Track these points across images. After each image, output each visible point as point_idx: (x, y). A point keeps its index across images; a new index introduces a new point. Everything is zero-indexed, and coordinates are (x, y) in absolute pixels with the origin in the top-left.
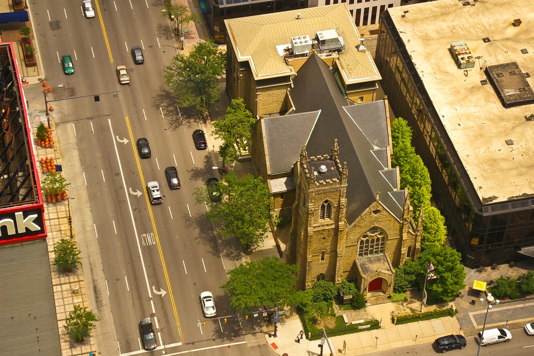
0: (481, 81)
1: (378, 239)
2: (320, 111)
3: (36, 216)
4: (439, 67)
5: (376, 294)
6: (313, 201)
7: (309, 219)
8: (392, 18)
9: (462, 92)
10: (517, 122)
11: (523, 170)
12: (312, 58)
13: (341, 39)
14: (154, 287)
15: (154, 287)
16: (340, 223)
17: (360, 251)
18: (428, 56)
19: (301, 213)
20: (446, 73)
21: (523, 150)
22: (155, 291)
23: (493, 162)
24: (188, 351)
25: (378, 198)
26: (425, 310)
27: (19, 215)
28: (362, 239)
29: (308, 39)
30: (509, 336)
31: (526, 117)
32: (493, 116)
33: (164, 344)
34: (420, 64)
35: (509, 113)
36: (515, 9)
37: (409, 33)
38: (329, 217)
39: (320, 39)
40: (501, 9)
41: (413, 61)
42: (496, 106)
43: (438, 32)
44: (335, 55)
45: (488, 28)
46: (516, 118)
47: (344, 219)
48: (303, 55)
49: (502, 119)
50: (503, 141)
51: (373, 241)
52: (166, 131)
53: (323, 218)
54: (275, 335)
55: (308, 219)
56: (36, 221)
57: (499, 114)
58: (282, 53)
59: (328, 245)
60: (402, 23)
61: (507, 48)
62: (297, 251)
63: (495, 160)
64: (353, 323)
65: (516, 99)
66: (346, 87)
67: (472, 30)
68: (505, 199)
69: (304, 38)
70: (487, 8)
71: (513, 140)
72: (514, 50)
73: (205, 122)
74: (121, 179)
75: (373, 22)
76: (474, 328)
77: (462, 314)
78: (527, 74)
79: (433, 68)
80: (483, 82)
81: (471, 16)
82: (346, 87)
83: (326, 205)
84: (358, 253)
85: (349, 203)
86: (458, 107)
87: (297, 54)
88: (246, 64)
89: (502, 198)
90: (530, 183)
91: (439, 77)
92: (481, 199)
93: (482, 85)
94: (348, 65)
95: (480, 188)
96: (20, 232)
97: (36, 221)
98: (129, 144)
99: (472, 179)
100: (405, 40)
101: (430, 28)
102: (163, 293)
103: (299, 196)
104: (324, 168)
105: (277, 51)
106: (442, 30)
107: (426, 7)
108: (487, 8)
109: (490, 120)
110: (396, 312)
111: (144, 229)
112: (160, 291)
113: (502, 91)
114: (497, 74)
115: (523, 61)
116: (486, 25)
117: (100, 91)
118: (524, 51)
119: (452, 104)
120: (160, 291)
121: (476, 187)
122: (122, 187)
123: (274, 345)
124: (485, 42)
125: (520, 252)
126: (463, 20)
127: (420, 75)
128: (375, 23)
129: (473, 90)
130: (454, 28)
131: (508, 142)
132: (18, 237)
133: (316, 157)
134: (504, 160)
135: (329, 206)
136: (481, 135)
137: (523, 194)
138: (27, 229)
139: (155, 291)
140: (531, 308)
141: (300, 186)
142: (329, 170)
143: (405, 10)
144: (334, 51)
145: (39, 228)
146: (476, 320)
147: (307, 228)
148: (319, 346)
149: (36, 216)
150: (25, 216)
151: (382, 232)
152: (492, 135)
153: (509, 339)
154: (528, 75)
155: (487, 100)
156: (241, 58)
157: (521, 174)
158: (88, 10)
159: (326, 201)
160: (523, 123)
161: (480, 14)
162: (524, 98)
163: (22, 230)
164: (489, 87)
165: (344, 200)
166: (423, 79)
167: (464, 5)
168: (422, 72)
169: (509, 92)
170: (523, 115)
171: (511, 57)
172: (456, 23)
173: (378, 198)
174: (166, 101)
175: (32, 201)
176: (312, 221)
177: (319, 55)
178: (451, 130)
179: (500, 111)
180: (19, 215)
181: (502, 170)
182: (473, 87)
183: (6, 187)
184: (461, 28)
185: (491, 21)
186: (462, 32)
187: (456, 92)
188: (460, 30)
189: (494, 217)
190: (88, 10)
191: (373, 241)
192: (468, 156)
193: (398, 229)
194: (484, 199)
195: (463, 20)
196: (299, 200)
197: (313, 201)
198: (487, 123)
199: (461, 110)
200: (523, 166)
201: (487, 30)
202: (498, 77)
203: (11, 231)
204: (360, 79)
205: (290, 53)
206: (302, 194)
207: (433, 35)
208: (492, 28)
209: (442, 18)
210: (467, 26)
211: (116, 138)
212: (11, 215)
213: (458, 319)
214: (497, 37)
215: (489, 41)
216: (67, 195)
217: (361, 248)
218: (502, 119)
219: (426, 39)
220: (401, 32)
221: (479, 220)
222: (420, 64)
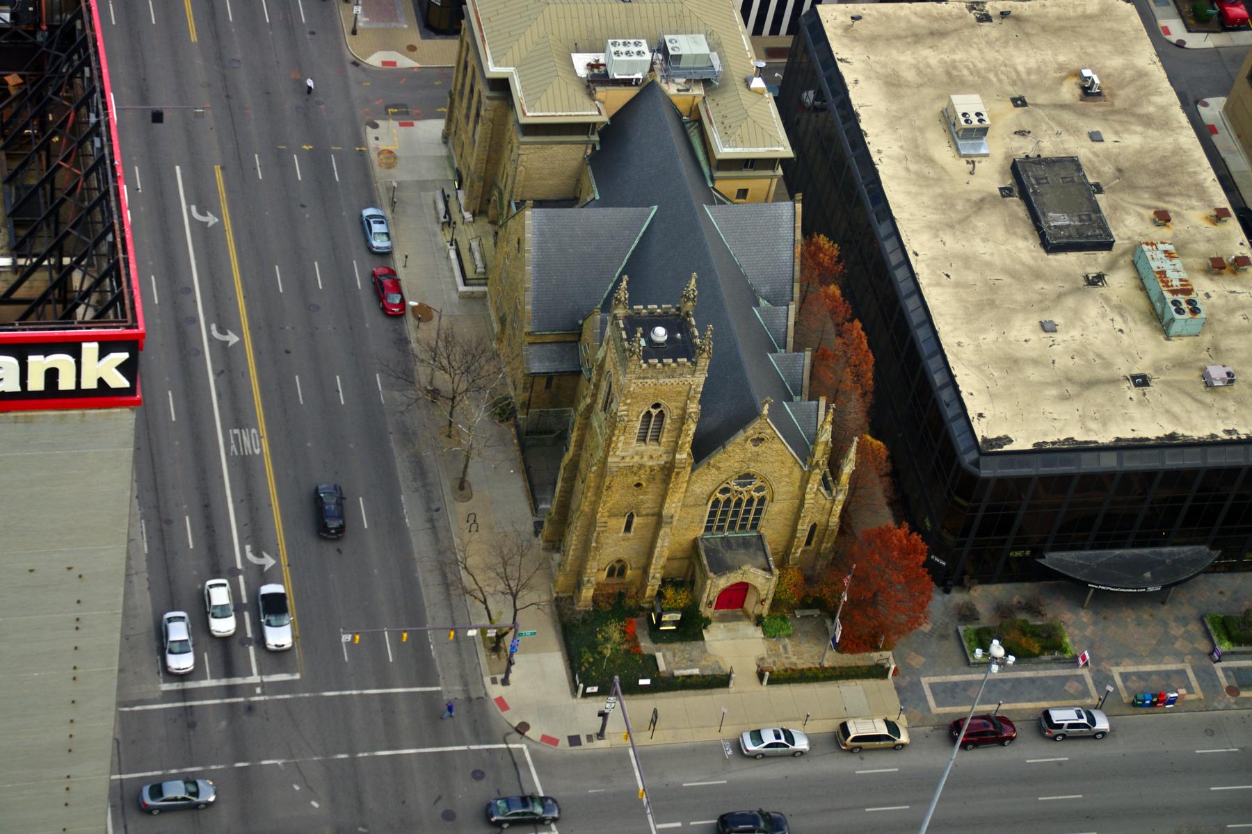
0: (1001, 189)
2: (656, 207)
3: (125, 356)
4: (917, 146)
8: (826, 26)
9: (960, 207)
10: (1067, 286)
11: (1072, 389)
13: (715, 57)
14: (248, 548)
15: (248, 548)
16: (678, 456)
17: (708, 522)
18: (893, 122)
19: (595, 424)
20: (930, 161)
21: (1074, 346)
22: (250, 556)
23: (1012, 363)
24: (337, 693)
25: (765, 412)
26: (831, 659)
27: (90, 350)
29: (644, 47)
30: (904, 738)
31: (1087, 277)
32: (1018, 267)
33: (261, 673)
34: (877, 136)
35: (1054, 263)
36: (1084, 43)
37: (858, 65)
38: (656, 439)
39: (671, 52)
40: (1054, 40)
41: (863, 126)
42: (1026, 249)
43: (919, 72)
44: (698, 91)
45: (1024, 76)
46: (1067, 276)
47: (687, 448)
48: (627, 83)
49: (1038, 275)
50: (1034, 321)
51: (738, 504)
52: (303, 210)
53: (644, 441)
54: (505, 682)
55: (610, 438)
56: (122, 368)
57: (1032, 263)
58: (582, 72)
59: (648, 499)
60: (846, 41)
61: (1060, 124)
62: (574, 506)
63: (1016, 361)
64: (677, 673)
65: (1069, 237)
66: (714, 164)
67: (992, 76)
68: (1029, 447)
69: (636, 44)
70: (1027, 34)
71: (1056, 321)
72: (1075, 131)
73: (9, 216)
74: (195, 302)
75: (775, 30)
76: (929, 710)
77: (908, 679)
78: (1097, 186)
79: (901, 147)
80: (1006, 192)
81: (990, 43)
82: (714, 164)
83: (654, 412)
85: (704, 413)
86: (948, 238)
87: (617, 77)
88: (501, 86)
89: (1022, 442)
90: (1082, 418)
91: (913, 167)
92: (979, 439)
93: (1003, 196)
94: (724, 117)
95: (980, 415)
96: (84, 386)
97: (122, 368)
98: (220, 226)
99: (964, 395)
100: (848, 78)
101: (905, 59)
103: (597, 386)
104: (660, 333)
105: (572, 65)
106: (928, 66)
107: (902, 13)
108: (1027, 34)
109: (1013, 274)
110: (770, 661)
111: (238, 417)
112: (262, 557)
113: (1044, 214)
114: (1037, 179)
115: (1091, 156)
116: (1021, 68)
117: (162, 99)
118: (1096, 137)
119: (934, 229)
120: (262, 557)
121: (972, 413)
122: (195, 320)
123: (501, 702)
124: (1016, 106)
125: (1042, 561)
126: (974, 52)
127: (875, 159)
129: (981, 204)
130: (955, 68)
131: (1048, 326)
132: (79, 397)
133: (645, 308)
134: (1035, 362)
135: (661, 415)
136: (992, 304)
137: (1067, 440)
138: (101, 381)
139: (250, 556)
140: (1050, 682)
141: (601, 367)
142: (671, 339)
143: (855, 14)
144: (697, 81)
145: (125, 383)
146: (935, 695)
147: (606, 459)
148: (600, 715)
149: (125, 356)
150: (102, 354)
152: (1013, 306)
153: (903, 745)
154: (1099, 188)
155: (1010, 230)
156: (494, 70)
157: (1065, 398)
159: (656, 406)
160: (1079, 289)
161: (1011, 43)
162: (1088, 237)
163: (89, 383)
164: (1016, 206)
165: (694, 408)
166: (879, 167)
167: (980, 20)
168: (879, 152)
169: (1058, 220)
170: (1080, 272)
171: (1067, 146)
172: (958, 56)
173: (765, 412)
174: (1151, 109)
175: (122, 320)
177: (664, 86)
178: (929, 285)
179: (1033, 258)
180: (90, 350)
181: (1028, 384)
182: (982, 200)
183: (53, 287)
184: (968, 68)
185: (1032, 63)
186: (971, 78)
187: (947, 202)
188: (966, 72)
189: (1001, 481)
191: (738, 504)
192: (959, 344)
193: (798, 484)
194: (985, 440)
195: (974, 52)
196: (594, 396)
198: (1007, 279)
199: (953, 244)
200: (1069, 380)
201: (1022, 81)
202: (1038, 184)
203: (66, 382)
204: (746, 150)
205: (599, 78)
206: (604, 385)
207: (910, 75)
208: (1033, 77)
209: (929, 41)
210: (981, 65)
211: (189, 211)
212: (74, 349)
214: (1042, 99)
215: (1024, 104)
217: (712, 514)
218: (1038, 275)
219: (892, 84)
220: (841, 60)
221: (969, 483)
222: (877, 136)
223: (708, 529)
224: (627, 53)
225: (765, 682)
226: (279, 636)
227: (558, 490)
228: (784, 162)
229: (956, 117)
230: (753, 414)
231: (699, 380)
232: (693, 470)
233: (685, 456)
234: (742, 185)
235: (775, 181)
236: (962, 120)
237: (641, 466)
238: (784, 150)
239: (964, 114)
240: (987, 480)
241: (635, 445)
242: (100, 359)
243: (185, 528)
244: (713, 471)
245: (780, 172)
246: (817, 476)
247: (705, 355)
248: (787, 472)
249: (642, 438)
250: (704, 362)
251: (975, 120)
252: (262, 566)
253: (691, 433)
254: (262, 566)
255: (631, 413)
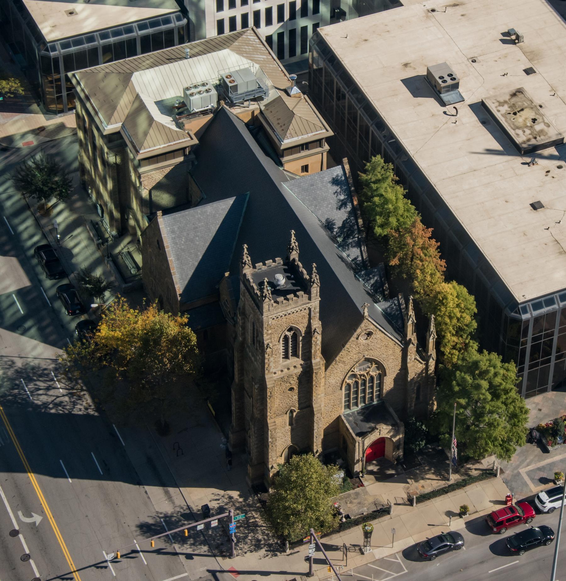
1: (372, 378)
5: (323, 466)
6: (270, 332)
7: (266, 361)
12: (219, 116)
14: (20, 513)
28: (348, 381)
38: (295, 354)
47: (319, 354)
51: (364, 384)
75: (292, 52)
83: (289, 334)
84: (343, 404)
87: (197, 111)
102: (37, 519)
103: (244, 328)
120: (32, 516)
128: (295, 55)
151: (380, 366)
158: (358, 268)
165: (317, 324)
173: (366, 314)
176: (271, 364)
190: (358, 268)
197: (270, 332)
206: (249, 327)
213: (506, 482)
216: (534, 422)
217: (348, 395)
223: (348, 407)
224: (199, 93)
225: (415, 504)
226: (344, 520)
227: (233, 408)
228: (329, 140)
229: (436, 80)
230: (361, 318)
231: (315, 303)
232: (326, 369)
233: (318, 359)
234: (303, 162)
235: (325, 154)
236: (440, 81)
237: (289, 376)
238: (326, 132)
239: (440, 78)
240: (528, 321)
241: (282, 362)
242: (401, 80)
243: (98, 469)
244: (340, 365)
245: (327, 147)
246: (412, 349)
247: (315, 285)
248: (391, 352)
249: (286, 357)
250: (315, 290)
251: (448, 79)
252: (34, 523)
253: (319, 342)
254: (34, 523)
255: (273, 340)
